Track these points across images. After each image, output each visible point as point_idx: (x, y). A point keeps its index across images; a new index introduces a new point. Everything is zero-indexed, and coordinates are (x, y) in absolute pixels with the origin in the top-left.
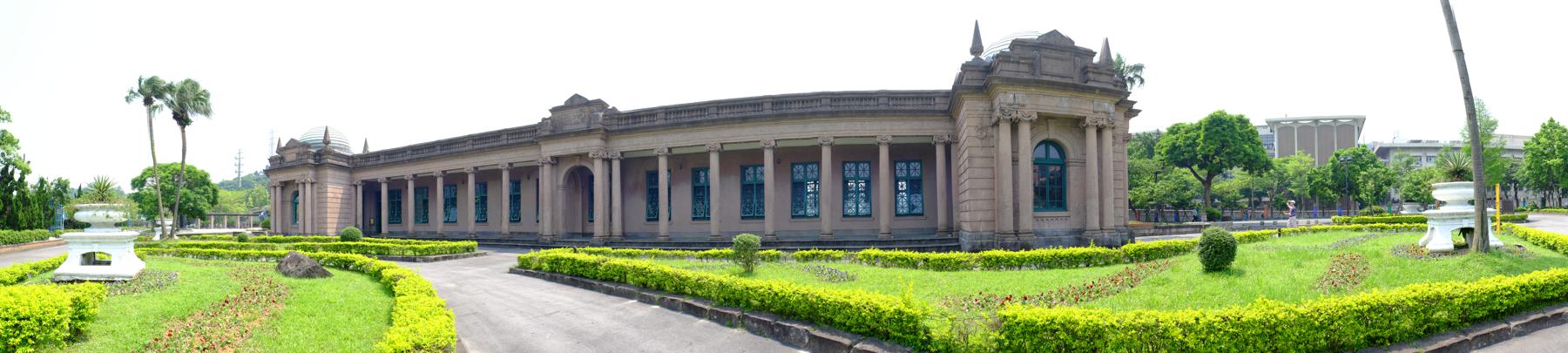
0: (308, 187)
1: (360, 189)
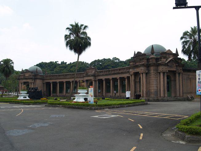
0: (144, 75)
1: (45, 84)
